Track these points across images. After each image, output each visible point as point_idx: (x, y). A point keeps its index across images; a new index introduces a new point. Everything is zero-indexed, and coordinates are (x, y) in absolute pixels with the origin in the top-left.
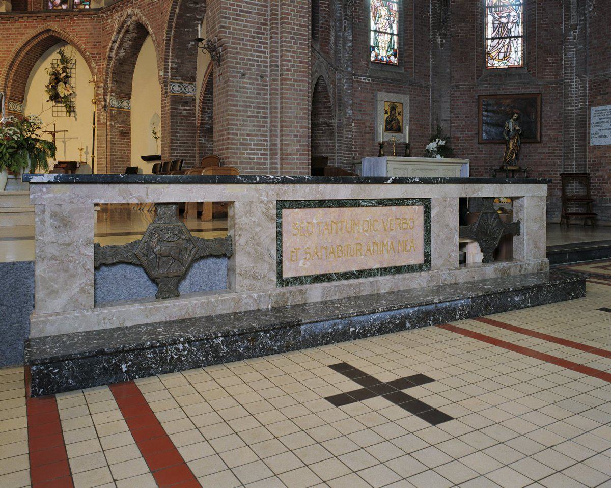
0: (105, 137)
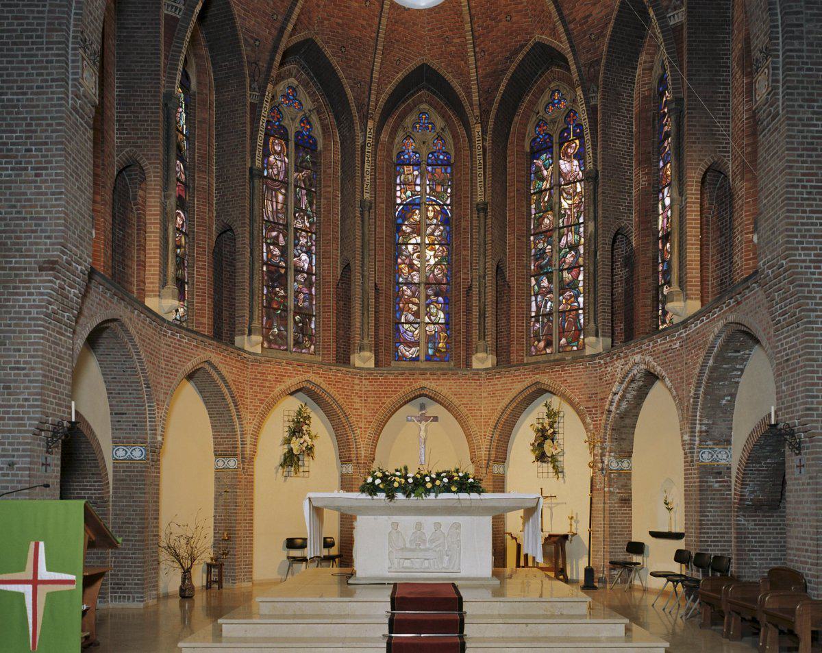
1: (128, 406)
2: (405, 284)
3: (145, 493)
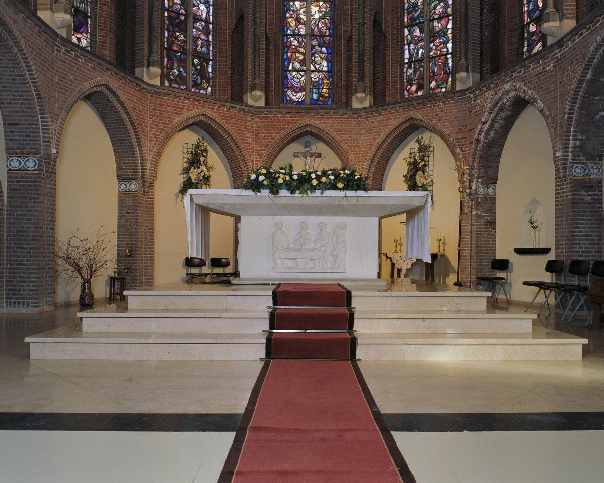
0: (470, 227)
1: (19, 116)
2: (293, 36)
3: (39, 203)
